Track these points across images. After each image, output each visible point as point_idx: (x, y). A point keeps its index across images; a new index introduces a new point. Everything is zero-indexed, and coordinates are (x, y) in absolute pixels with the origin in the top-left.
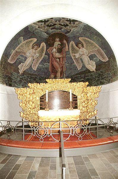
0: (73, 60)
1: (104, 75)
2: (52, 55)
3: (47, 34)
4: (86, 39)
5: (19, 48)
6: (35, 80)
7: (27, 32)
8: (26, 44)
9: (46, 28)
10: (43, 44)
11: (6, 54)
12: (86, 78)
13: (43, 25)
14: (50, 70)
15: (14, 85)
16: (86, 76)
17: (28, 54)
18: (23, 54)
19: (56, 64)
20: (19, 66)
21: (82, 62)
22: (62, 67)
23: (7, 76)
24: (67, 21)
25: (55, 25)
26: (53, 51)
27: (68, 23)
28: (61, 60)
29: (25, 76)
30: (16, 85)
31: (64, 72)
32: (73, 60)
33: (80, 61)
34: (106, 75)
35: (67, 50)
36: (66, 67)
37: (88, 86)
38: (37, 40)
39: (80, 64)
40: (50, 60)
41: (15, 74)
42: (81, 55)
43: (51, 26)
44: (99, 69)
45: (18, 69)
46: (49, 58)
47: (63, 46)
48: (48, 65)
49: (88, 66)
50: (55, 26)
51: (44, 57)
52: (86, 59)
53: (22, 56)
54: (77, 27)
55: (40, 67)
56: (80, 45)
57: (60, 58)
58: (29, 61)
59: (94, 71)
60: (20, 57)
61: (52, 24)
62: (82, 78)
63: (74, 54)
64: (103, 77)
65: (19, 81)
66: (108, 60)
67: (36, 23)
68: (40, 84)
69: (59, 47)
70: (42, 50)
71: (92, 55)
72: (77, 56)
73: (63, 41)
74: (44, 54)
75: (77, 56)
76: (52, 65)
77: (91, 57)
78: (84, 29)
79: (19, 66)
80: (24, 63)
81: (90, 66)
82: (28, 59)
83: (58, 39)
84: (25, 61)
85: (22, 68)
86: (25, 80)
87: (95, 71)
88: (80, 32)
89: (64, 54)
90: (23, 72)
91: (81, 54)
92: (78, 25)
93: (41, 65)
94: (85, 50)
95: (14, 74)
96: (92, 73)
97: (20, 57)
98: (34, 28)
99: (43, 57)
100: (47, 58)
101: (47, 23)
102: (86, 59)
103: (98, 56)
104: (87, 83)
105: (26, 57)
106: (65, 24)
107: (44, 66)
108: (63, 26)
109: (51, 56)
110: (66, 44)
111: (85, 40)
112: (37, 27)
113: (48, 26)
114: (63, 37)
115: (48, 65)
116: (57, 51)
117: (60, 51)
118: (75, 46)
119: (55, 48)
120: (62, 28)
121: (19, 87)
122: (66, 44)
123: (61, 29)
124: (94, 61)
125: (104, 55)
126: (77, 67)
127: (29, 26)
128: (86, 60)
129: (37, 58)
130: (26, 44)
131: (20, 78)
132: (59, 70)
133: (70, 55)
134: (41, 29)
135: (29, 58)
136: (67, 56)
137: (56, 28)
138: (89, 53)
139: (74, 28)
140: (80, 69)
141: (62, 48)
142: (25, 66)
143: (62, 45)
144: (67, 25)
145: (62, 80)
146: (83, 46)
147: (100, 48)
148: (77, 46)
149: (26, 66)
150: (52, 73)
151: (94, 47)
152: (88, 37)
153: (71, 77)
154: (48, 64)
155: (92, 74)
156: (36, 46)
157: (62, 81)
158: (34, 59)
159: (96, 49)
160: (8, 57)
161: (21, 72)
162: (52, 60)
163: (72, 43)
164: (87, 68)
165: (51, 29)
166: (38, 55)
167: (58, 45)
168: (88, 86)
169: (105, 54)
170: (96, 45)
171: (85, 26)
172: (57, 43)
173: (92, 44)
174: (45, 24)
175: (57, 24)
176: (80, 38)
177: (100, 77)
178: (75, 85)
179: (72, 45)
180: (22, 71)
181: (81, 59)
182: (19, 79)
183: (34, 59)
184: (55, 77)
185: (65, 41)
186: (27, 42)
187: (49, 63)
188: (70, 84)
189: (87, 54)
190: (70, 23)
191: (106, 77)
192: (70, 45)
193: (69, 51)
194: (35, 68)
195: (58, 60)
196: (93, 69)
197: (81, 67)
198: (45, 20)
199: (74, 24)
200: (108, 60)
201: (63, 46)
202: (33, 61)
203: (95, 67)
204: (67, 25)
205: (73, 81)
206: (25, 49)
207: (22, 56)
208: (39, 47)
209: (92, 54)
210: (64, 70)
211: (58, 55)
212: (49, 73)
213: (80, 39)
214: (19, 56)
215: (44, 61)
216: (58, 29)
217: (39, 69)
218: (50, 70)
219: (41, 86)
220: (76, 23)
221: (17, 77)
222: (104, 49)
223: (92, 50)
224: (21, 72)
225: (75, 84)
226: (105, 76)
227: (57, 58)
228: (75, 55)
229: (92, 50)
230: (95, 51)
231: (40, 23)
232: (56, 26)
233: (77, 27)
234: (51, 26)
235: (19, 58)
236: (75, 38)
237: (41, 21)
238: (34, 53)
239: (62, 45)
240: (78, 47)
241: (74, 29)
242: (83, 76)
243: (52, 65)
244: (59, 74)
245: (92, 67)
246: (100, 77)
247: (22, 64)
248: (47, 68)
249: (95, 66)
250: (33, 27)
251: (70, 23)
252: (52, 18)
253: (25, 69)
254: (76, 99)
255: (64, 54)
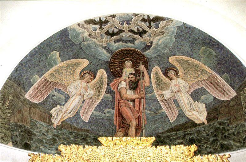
0: (158, 103)
1: (228, 130)
2: (120, 94)
3: (108, 51)
4: (184, 57)
5: (52, 75)
6: (84, 140)
7: (64, 43)
8: (67, 69)
9: (106, 38)
10: (102, 73)
11: (19, 78)
12: (188, 137)
13: (97, 31)
14: (115, 122)
15: (36, 147)
16: (188, 134)
17: (71, 89)
18: (62, 88)
19: (127, 112)
20: (53, 111)
21: (178, 106)
22: (139, 117)
23: (21, 127)
24: (144, 20)
25: (121, 31)
26: (122, 86)
27: (145, 26)
28: (137, 103)
29: (64, 131)
30: (41, 147)
31: (143, 128)
32: (160, 102)
33: (173, 105)
34: (233, 130)
35: (148, 84)
36: (147, 118)
37: (196, 153)
38: (90, 63)
39: (173, 111)
40: (116, 103)
41: (42, 126)
42: (174, 94)
43: (113, 34)
44: (215, 118)
45: (50, 115)
46: (113, 99)
47: (139, 76)
48: (112, 113)
49: (191, 114)
50: (121, 34)
51: (105, 97)
52: (185, 100)
53: (59, 91)
54: (165, 35)
55: (95, 116)
56: (172, 73)
57: (135, 100)
58: (73, 103)
59: (203, 124)
60: (56, 93)
61: (116, 30)
62: (178, 138)
63: (160, 92)
64: (226, 134)
65: (51, 139)
66: (235, 94)
67: (83, 25)
68: (84, 147)
69: (132, 79)
70: (100, 84)
71: (197, 89)
72: (167, 94)
73: (139, 67)
74: (104, 92)
75: (167, 94)
76: (120, 114)
77: (196, 96)
78: (178, 36)
79: (53, 111)
80: (64, 105)
81: (195, 113)
82: (71, 100)
83: (128, 63)
84: (66, 102)
85: (59, 115)
86: (64, 139)
87: (206, 123)
88: (171, 45)
89: (143, 93)
90: (60, 124)
91: (175, 90)
92: (166, 29)
93: (96, 113)
94: (182, 81)
95: (40, 124)
96: (201, 128)
97: (56, 93)
98: (81, 36)
99: (101, 97)
100: (109, 100)
101: (106, 28)
102: (185, 100)
103: (209, 91)
104: (194, 148)
105: (68, 95)
106: (141, 30)
107: (103, 115)
108: (136, 33)
109: (117, 96)
110: (146, 73)
111: (181, 62)
112: (86, 34)
113: (107, 33)
114: (137, 58)
115: (112, 113)
116: (128, 87)
117: (134, 86)
118: (162, 75)
119: (125, 81)
120: (136, 39)
121: (49, 151)
122: (146, 73)
123: (133, 41)
124: (202, 102)
125: (224, 85)
126: (167, 117)
127: (70, 30)
128: (186, 101)
129: (91, 98)
130: (67, 69)
131: (54, 135)
132: (134, 123)
133: (153, 94)
134: (95, 40)
135: (74, 98)
136: (147, 95)
137: (123, 38)
138: (190, 88)
139: (158, 37)
140: (174, 120)
141: (139, 80)
142: (66, 112)
143: (138, 73)
144: (144, 32)
145: (136, 140)
146: (177, 73)
147: (214, 73)
148: (166, 74)
149: (68, 112)
150: (119, 128)
151: (199, 73)
152: (187, 54)
153: (158, 137)
154: (112, 110)
155: (199, 129)
156: (87, 77)
157: (135, 142)
158: (84, 101)
159: (205, 77)
160: (24, 88)
161: (56, 122)
162: (119, 103)
163: (156, 69)
164: (188, 118)
165: (115, 42)
166: (92, 92)
167: (130, 74)
168: (196, 153)
169: (225, 83)
170: (206, 68)
171: (179, 28)
172: (128, 70)
173: (196, 67)
174: (101, 28)
175: (124, 29)
176: (170, 58)
177: (220, 135)
178: (166, 151)
179: (157, 74)
180: (59, 122)
181: (176, 101)
182: (50, 136)
183: (84, 101)
184: (126, 135)
185: (142, 67)
186: (68, 65)
187: (113, 109)
188: (155, 148)
189: (187, 90)
190: (149, 27)
191: (234, 133)
192: (152, 75)
193: (150, 87)
194: (86, 118)
195: (131, 103)
196: (201, 118)
197: (176, 117)
198: (100, 19)
199: (157, 26)
200: (235, 94)
201: (139, 76)
202: (83, 103)
203: (205, 114)
204: (144, 32)
205: (160, 141)
206: (65, 79)
207: (59, 91)
208: (94, 78)
209: (197, 88)
210: (143, 123)
211: (130, 94)
212: (114, 128)
213: (172, 60)
214: (52, 92)
215: (103, 105)
216: (127, 41)
217: (93, 120)
218: (116, 123)
219: (87, 151)
220: (162, 24)
221: (47, 131)
222: (223, 73)
223: (196, 80)
224: (56, 122)
225: (164, 149)
226: (231, 131)
227: (128, 100)
228: (164, 92)
229: (196, 80)
230: (204, 80)
231: (92, 26)
232: (123, 34)
233: (164, 33)
234: (113, 34)
235: (52, 94)
236: (162, 59)
237: (92, 22)
238: (84, 88)
239: (138, 73)
240: (169, 78)
241: (159, 40)
242: (181, 133)
243: (120, 114)
244: (132, 130)
245: (198, 114)
246: (220, 135)
247: (58, 106)
248: (109, 119)
249: (206, 112)
250: (78, 35)
251: (149, 27)
252: (113, 16)
253: (65, 119)
254: (132, 130)
255: (143, 93)
